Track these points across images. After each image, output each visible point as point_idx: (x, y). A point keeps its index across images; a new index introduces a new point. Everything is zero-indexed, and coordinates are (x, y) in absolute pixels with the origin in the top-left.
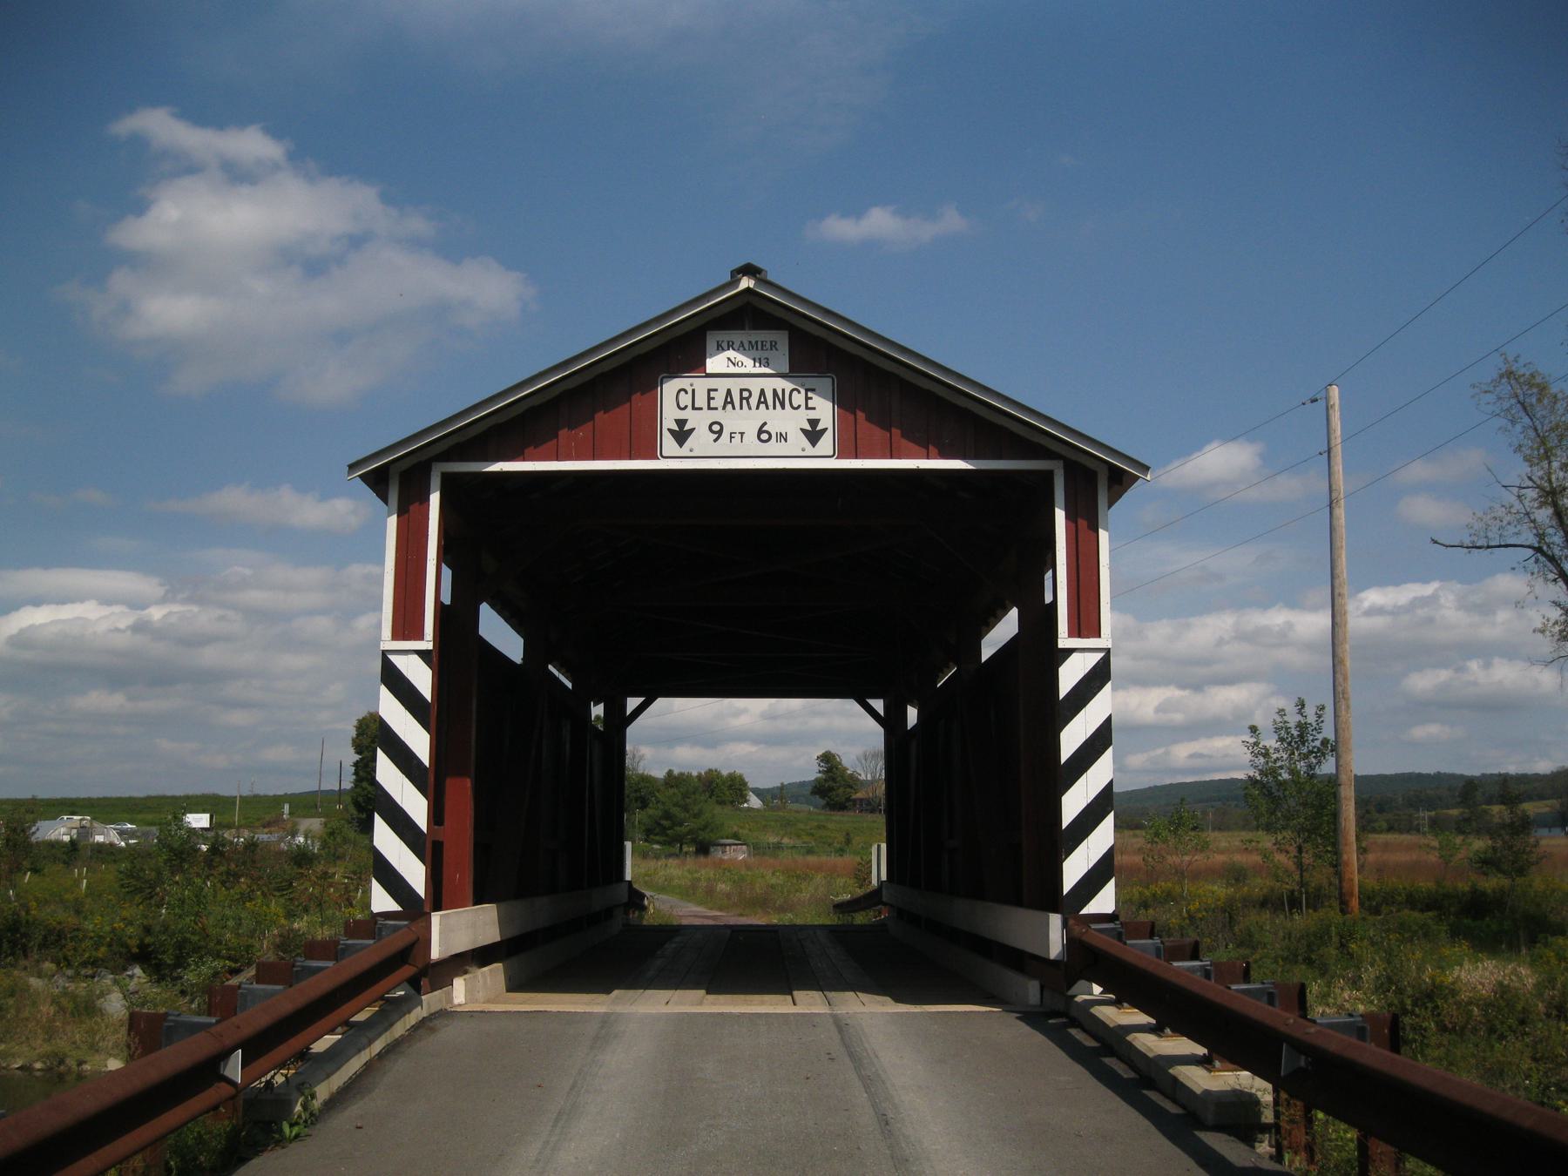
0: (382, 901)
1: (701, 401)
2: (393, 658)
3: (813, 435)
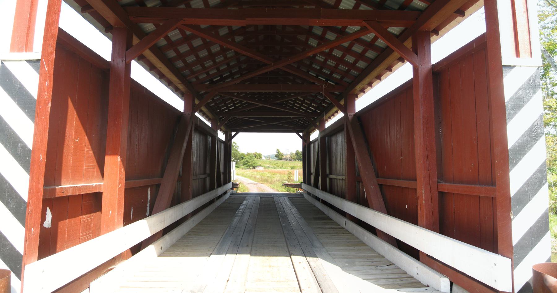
2: (4, 62)
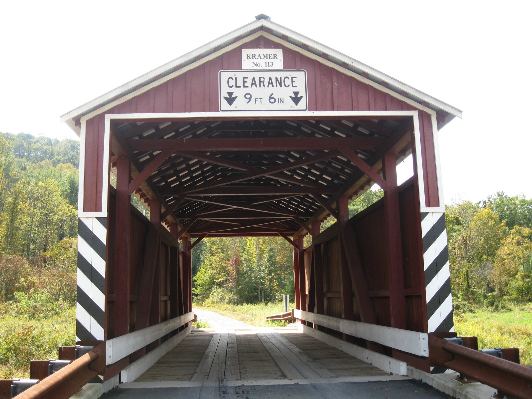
1: (240, 83)
3: (296, 99)
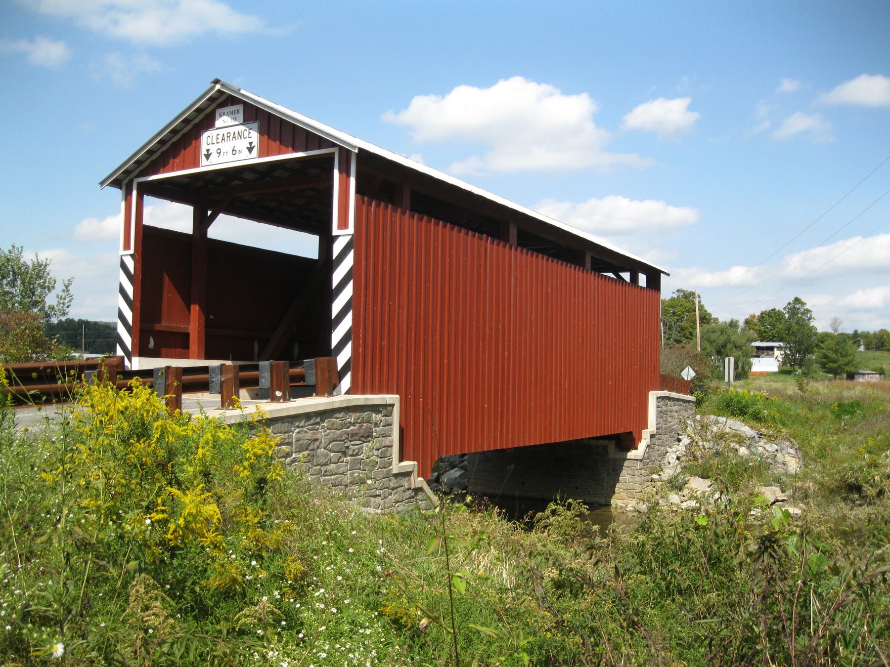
0: (120, 352)
3: (250, 149)
